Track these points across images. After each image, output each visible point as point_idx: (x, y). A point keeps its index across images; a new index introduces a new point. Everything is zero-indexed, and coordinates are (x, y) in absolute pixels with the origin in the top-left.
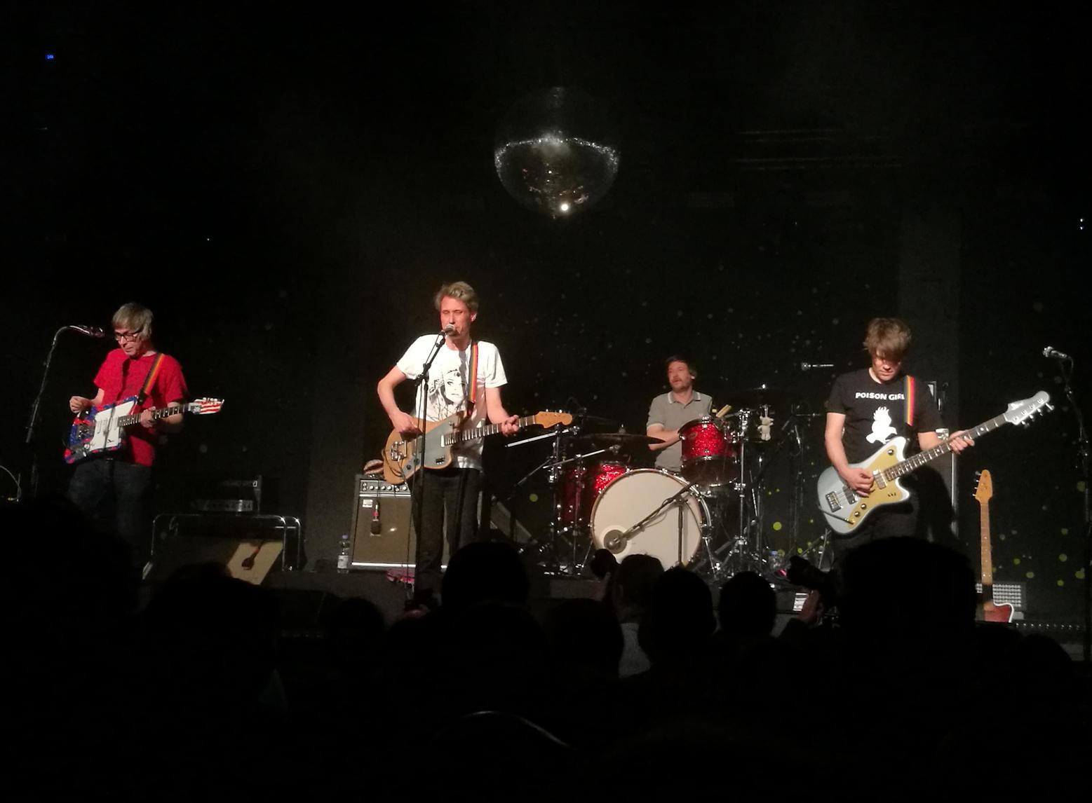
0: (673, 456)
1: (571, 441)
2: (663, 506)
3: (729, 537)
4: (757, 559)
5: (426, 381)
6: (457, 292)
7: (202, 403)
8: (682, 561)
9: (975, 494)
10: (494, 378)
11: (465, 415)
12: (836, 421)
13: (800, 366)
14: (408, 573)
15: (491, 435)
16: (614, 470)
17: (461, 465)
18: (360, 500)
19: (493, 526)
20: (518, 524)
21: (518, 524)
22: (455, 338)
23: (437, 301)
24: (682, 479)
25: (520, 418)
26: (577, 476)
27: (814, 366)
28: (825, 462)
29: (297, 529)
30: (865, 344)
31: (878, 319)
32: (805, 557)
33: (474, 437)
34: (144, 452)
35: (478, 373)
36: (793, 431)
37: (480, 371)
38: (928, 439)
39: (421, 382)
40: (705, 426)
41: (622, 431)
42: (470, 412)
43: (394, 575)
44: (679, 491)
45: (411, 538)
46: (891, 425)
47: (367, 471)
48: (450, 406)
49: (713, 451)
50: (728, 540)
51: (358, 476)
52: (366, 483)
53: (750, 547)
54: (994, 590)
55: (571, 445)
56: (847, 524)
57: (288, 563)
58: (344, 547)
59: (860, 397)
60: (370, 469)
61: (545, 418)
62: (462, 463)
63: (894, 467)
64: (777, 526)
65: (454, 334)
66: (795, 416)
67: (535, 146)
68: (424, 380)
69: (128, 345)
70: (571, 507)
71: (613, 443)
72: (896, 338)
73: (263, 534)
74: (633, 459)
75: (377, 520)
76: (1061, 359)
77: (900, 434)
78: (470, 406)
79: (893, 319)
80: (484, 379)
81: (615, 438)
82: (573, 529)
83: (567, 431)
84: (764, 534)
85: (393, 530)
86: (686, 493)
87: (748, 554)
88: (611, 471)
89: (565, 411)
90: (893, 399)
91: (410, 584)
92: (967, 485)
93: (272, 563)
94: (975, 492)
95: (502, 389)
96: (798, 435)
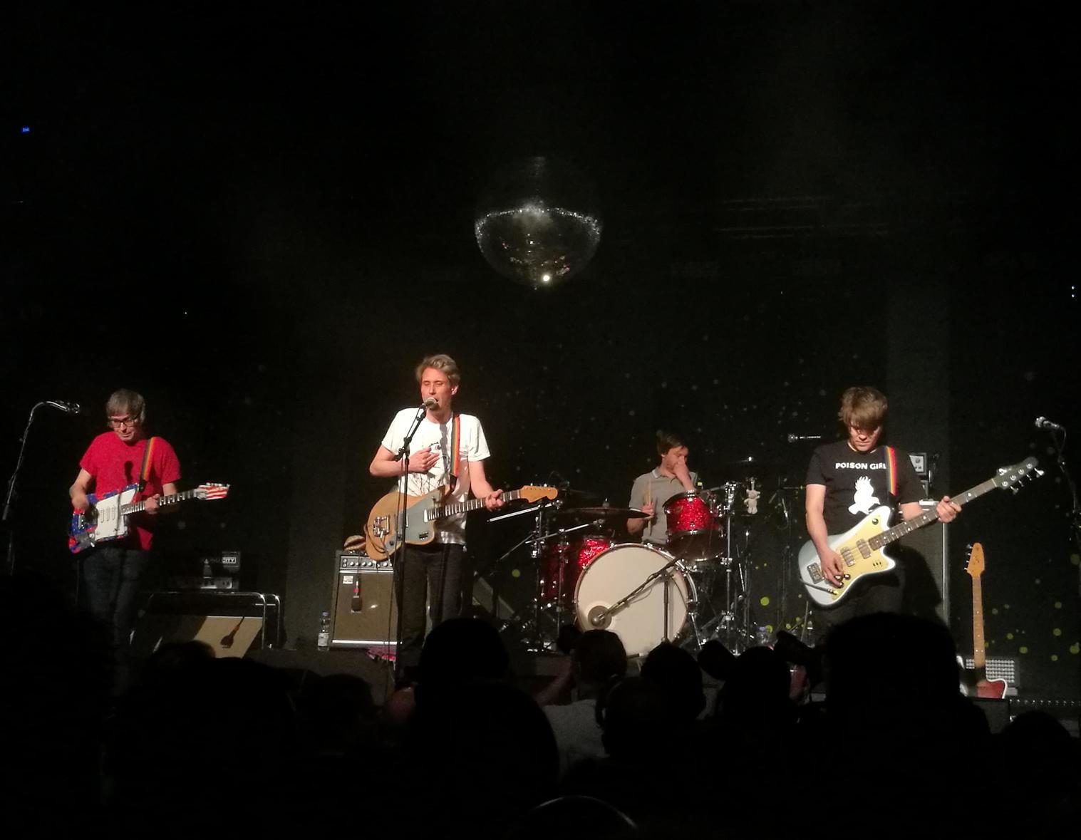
0: (660, 530)
1: (554, 515)
2: (648, 581)
3: (715, 613)
4: (745, 635)
5: (407, 456)
6: (438, 363)
7: (207, 488)
8: (668, 637)
9: (967, 567)
10: (477, 451)
11: (448, 489)
12: (816, 493)
13: (786, 437)
14: (389, 651)
15: (474, 510)
16: (598, 545)
17: (446, 541)
18: (340, 576)
19: (475, 603)
20: (501, 601)
21: (501, 601)
22: (438, 412)
23: (418, 373)
24: (667, 554)
25: (504, 492)
26: (560, 551)
27: (801, 438)
28: (808, 537)
29: (277, 604)
30: (840, 414)
31: (853, 388)
32: (794, 633)
33: (456, 512)
34: (146, 537)
35: (461, 446)
36: (780, 504)
37: (462, 444)
38: (910, 510)
39: (402, 457)
40: (691, 500)
41: (606, 505)
42: (453, 487)
43: (375, 653)
44: (665, 565)
45: (393, 612)
46: (873, 495)
47: (348, 546)
48: (432, 479)
49: (698, 525)
50: (713, 616)
51: (339, 552)
52: (347, 559)
53: (737, 623)
54: (987, 669)
55: (554, 520)
56: (830, 595)
57: (268, 640)
58: (325, 624)
59: (840, 468)
60: (351, 544)
61: (530, 492)
62: (445, 538)
63: (879, 535)
64: (765, 601)
65: (435, 408)
66: (782, 489)
67: (516, 216)
68: (404, 454)
69: (123, 428)
70: (555, 582)
71: (598, 517)
72: (872, 407)
73: (242, 607)
74: (616, 534)
75: (358, 597)
76: (1054, 429)
77: (883, 503)
78: (453, 480)
79: (867, 388)
80: (467, 453)
81: (598, 512)
82: (557, 605)
83: (550, 505)
84: (751, 612)
85: (373, 606)
86: (671, 568)
87: (735, 630)
88: (596, 545)
89: (550, 485)
90: (874, 468)
91: (392, 662)
92: (958, 559)
93: (253, 639)
94: (967, 565)
95: (487, 464)
96: (785, 508)
